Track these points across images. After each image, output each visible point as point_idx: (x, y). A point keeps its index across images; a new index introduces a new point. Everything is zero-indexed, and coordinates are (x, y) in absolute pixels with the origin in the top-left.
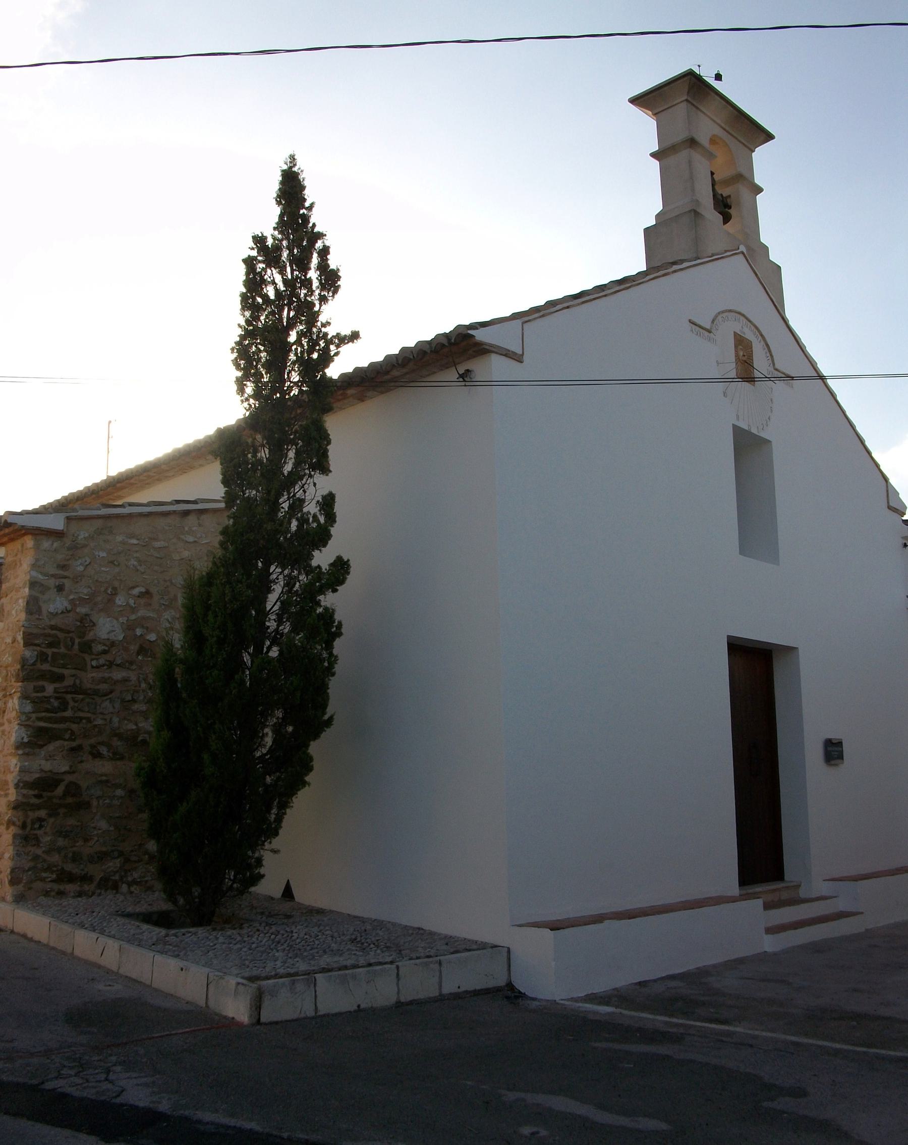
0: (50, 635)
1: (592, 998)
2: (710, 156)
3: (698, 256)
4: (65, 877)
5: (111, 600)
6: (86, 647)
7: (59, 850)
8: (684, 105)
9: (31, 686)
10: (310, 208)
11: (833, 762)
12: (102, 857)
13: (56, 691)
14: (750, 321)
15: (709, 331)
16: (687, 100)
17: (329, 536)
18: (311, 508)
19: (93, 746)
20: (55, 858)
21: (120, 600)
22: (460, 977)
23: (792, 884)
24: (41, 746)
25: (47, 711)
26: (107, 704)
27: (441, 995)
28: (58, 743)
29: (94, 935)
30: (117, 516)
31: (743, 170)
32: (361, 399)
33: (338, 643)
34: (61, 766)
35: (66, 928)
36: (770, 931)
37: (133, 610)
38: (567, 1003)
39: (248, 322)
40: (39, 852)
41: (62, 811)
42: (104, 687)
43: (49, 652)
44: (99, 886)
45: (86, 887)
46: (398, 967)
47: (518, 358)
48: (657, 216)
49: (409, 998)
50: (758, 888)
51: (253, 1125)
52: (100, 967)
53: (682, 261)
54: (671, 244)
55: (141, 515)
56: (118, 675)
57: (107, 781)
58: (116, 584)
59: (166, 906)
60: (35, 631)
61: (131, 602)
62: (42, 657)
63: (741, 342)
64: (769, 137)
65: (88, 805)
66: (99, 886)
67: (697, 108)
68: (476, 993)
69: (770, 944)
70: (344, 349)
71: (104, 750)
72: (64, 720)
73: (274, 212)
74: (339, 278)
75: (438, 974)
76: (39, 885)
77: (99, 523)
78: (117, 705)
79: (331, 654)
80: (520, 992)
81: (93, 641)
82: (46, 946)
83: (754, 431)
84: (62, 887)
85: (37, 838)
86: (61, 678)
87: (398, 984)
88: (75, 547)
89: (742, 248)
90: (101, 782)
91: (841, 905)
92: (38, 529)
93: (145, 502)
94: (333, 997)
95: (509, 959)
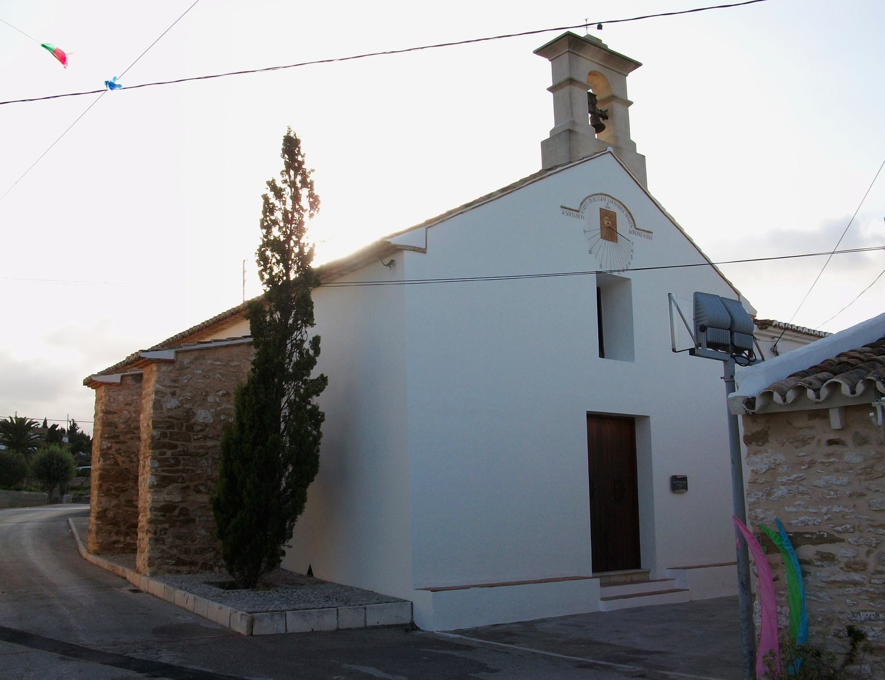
0: (167, 422)
3: (571, 161)
4: (180, 562)
5: (205, 399)
6: (190, 428)
7: (177, 547)
8: (567, 55)
9: (157, 452)
12: (203, 551)
13: (172, 454)
15: (578, 211)
17: (315, 363)
18: (307, 345)
19: (195, 486)
20: (174, 551)
21: (210, 399)
22: (376, 617)
24: (164, 487)
25: (168, 466)
26: (204, 461)
28: (175, 485)
29: (184, 592)
30: (208, 348)
31: (616, 92)
33: (323, 425)
34: (177, 498)
35: (171, 588)
37: (219, 404)
38: (514, 626)
39: (265, 237)
40: (165, 548)
41: (178, 524)
42: (201, 451)
43: (168, 431)
44: (201, 568)
45: (193, 568)
48: (551, 132)
51: (210, 671)
52: (185, 609)
53: (556, 167)
54: (561, 151)
55: (222, 347)
56: (210, 443)
57: (205, 507)
58: (208, 389)
59: (231, 579)
60: (159, 420)
61: (218, 400)
62: (164, 435)
65: (193, 521)
66: (201, 568)
68: (384, 627)
69: (602, 607)
71: (202, 488)
72: (178, 471)
76: (166, 567)
77: (196, 354)
78: (210, 461)
79: (319, 432)
81: (194, 424)
82: (163, 600)
84: (179, 568)
85: (163, 540)
86: (176, 447)
88: (182, 368)
89: (610, 149)
90: (201, 507)
91: (677, 585)
92: (159, 359)
93: (225, 338)
94: (328, 622)
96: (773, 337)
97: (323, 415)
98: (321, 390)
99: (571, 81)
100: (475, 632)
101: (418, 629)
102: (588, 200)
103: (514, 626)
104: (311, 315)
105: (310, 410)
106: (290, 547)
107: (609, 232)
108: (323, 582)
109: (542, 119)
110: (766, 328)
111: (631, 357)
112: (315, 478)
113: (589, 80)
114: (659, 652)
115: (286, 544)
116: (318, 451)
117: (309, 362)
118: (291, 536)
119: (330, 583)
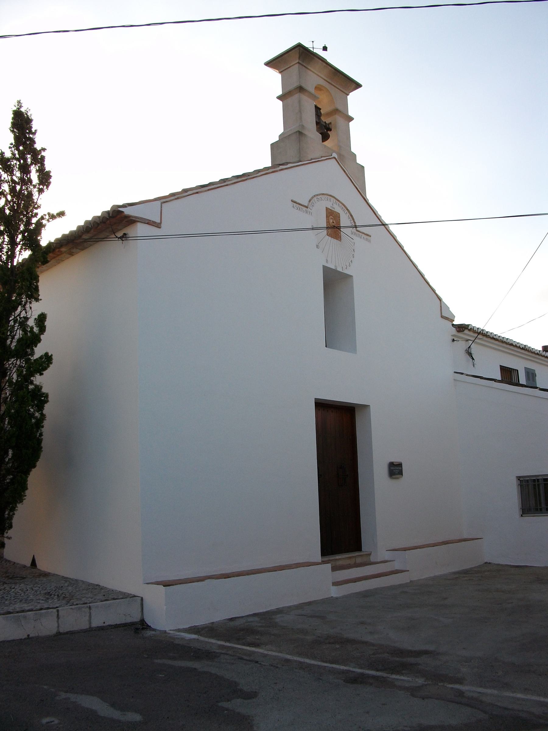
1: (179, 630)
2: (314, 97)
3: (301, 160)
8: (297, 65)
10: (34, 133)
11: (394, 477)
14: (338, 201)
15: (307, 207)
16: (298, 63)
17: (39, 340)
18: (31, 323)
22: (103, 616)
23: (367, 553)
27: (90, 628)
31: (340, 108)
32: (71, 254)
33: (47, 406)
36: (335, 584)
38: (251, 619)
46: (58, 611)
47: (158, 225)
48: (280, 136)
49: (100, 624)
50: (332, 557)
53: (287, 163)
54: (288, 152)
63: (330, 213)
64: (358, 86)
67: (305, 66)
69: (335, 592)
70: (53, 222)
73: (10, 138)
74: (50, 177)
75: (88, 614)
80: (148, 626)
83: (339, 269)
87: (58, 622)
89: (334, 155)
91: (397, 566)
94: (47, 626)
95: (142, 605)
96: (467, 340)
97: (47, 396)
98: (45, 369)
99: (301, 89)
100: (210, 630)
101: (148, 627)
102: (315, 199)
103: (251, 619)
104: (37, 289)
105: (33, 390)
106: (9, 538)
107: (334, 229)
108: (46, 575)
109: (272, 123)
110: (463, 331)
111: (353, 349)
112: (38, 464)
113: (315, 93)
114: (426, 652)
115: (6, 535)
116: (41, 435)
117: (33, 340)
118: (11, 527)
119: (54, 575)
